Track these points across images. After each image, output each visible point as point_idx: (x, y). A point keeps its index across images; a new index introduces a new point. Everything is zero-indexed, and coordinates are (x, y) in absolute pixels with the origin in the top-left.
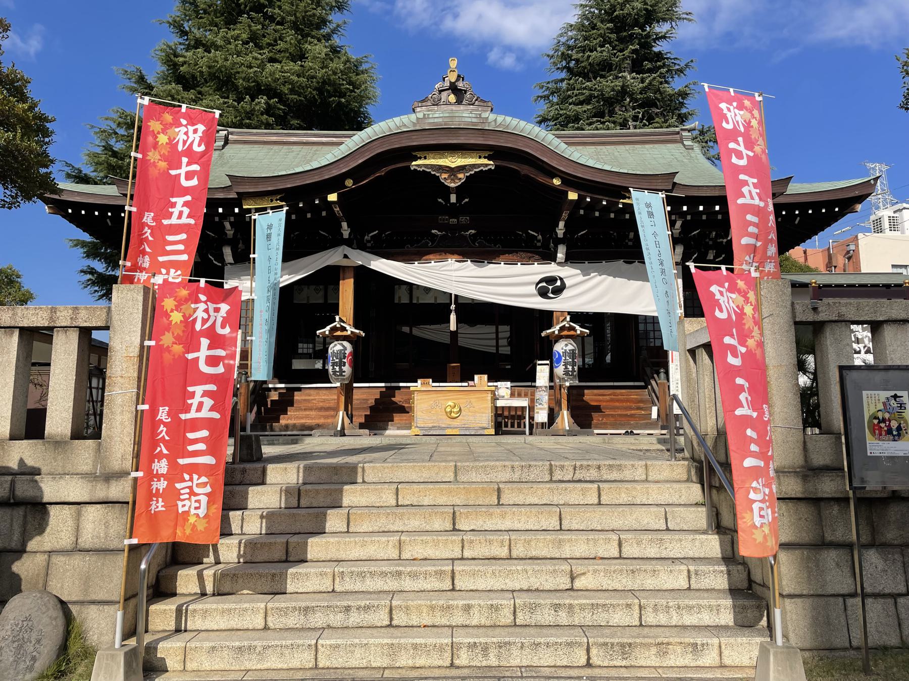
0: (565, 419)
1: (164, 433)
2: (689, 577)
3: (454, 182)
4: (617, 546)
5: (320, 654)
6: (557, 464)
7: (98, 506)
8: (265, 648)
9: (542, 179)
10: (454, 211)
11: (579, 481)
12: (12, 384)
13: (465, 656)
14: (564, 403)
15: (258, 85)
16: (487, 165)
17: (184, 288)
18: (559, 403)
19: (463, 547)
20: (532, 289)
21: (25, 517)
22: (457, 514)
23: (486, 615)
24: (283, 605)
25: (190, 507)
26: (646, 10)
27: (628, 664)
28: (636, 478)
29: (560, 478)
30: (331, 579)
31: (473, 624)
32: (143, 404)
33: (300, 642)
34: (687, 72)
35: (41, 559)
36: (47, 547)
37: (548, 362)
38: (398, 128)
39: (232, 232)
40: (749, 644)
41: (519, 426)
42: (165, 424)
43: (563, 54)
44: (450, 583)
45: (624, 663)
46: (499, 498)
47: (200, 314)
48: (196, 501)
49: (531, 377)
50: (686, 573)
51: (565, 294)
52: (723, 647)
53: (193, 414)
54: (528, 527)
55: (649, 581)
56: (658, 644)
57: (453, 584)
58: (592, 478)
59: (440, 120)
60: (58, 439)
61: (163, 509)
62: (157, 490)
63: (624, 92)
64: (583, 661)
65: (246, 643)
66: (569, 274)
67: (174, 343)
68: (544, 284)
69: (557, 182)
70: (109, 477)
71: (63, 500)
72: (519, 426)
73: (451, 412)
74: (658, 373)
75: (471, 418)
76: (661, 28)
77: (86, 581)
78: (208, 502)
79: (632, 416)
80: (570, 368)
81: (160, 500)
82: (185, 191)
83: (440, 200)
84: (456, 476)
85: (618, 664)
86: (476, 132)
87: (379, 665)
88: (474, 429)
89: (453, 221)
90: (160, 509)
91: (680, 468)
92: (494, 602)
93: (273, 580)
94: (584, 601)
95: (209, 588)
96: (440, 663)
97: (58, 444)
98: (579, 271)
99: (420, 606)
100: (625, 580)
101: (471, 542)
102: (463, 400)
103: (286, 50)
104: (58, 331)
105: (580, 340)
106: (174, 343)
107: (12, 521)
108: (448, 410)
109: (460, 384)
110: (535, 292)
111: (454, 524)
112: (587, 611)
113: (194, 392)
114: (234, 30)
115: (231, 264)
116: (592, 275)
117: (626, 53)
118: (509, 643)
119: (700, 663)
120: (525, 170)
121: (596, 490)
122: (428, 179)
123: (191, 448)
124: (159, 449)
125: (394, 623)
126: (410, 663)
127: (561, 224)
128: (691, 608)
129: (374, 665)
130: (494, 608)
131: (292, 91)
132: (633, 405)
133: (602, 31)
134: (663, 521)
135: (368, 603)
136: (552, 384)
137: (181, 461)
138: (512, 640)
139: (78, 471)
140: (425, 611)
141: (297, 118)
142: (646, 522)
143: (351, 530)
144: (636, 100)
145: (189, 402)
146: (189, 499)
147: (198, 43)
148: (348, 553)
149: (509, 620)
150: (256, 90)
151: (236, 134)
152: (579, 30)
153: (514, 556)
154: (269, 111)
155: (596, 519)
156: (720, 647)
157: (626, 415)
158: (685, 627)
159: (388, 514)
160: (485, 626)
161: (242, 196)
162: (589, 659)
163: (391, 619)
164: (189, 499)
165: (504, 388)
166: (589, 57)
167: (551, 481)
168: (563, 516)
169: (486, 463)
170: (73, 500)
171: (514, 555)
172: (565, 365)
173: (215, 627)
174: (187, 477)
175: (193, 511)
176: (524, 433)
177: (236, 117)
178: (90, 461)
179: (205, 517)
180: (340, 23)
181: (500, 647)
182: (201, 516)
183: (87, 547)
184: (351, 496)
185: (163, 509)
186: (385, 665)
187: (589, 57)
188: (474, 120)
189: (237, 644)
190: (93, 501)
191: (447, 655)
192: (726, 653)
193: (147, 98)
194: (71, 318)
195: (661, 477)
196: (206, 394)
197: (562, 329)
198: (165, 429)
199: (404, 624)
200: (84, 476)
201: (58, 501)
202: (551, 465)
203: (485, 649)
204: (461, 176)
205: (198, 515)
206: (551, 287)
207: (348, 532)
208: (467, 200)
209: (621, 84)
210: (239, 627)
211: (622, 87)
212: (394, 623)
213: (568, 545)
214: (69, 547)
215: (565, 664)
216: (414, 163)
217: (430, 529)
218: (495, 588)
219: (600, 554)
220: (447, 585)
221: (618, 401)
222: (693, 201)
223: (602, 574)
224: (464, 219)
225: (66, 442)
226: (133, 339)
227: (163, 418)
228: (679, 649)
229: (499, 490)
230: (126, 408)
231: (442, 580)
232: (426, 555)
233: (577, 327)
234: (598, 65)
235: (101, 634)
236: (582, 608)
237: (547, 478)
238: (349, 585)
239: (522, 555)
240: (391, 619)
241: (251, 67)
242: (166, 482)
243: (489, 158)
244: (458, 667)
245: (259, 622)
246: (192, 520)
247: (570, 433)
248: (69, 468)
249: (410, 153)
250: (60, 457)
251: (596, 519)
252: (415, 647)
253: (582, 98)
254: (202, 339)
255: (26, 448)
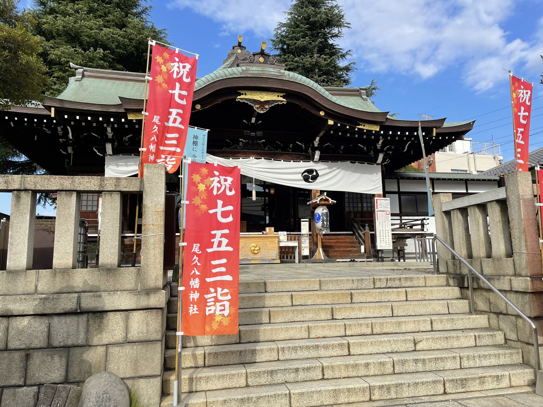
0: (320, 253)
1: (196, 261)
2: (475, 339)
3: (263, 110)
4: (430, 324)
5: (292, 399)
6: (378, 277)
7: (141, 311)
8: (258, 398)
9: (313, 111)
10: (254, 127)
11: (390, 288)
12: (73, 230)
13: (377, 394)
14: (320, 245)
15: (96, 41)
16: (282, 101)
17: (205, 167)
18: (316, 244)
19: (345, 329)
20: (300, 177)
21: (88, 321)
22: (334, 309)
23: (378, 368)
24: (257, 370)
25: (215, 310)
26: (328, 19)
27: (465, 391)
28: (420, 285)
29: (379, 286)
30: (276, 352)
31: (371, 374)
32: (183, 242)
33: (280, 393)
34: (347, 57)
35: (101, 350)
36: (105, 341)
37: (308, 220)
38: (231, 75)
39: (112, 134)
40: (523, 373)
41: (291, 258)
42: (198, 255)
43: (281, 40)
44: (347, 351)
45: (463, 390)
46: (351, 299)
47: (215, 184)
48: (220, 306)
49: (298, 228)
50: (474, 337)
51: (319, 180)
52: (511, 376)
53: (215, 248)
54: (376, 315)
55: (455, 343)
56: (480, 378)
57: (349, 351)
58: (396, 286)
59: (257, 72)
60: (109, 267)
61: (198, 312)
62: (193, 299)
63: (316, 64)
64: (442, 391)
65: (246, 396)
66: (321, 168)
67: (201, 204)
68: (306, 174)
69: (322, 113)
70: (149, 292)
71: (117, 308)
72: (291, 258)
73: (254, 250)
74: (364, 227)
75: (266, 253)
76: (335, 30)
77: (136, 363)
78: (230, 306)
79: (350, 251)
80: (325, 223)
81: (195, 306)
82: (179, 106)
83: (244, 121)
84: (320, 286)
85: (460, 391)
86: (279, 81)
87: (328, 403)
88: (268, 260)
89: (253, 134)
90: (195, 312)
91: (442, 279)
92: (382, 360)
93: (240, 355)
94: (431, 357)
95: (201, 362)
96: (364, 399)
97: (109, 270)
98: (326, 167)
99: (340, 365)
100: (443, 343)
101: (350, 325)
102: (261, 243)
103: (113, 21)
104: (106, 194)
105: (329, 207)
106: (201, 204)
107: (78, 325)
108: (252, 249)
109: (248, 233)
110: (302, 178)
111: (333, 315)
112: (432, 362)
113: (215, 234)
114: (78, 4)
115: (110, 155)
116: (334, 169)
117: (317, 43)
118: (402, 384)
119: (500, 386)
120: (304, 105)
121: (405, 292)
122: (247, 109)
123: (214, 271)
124: (193, 271)
125: (325, 377)
126: (346, 400)
127: (318, 139)
128: (485, 356)
129: (325, 404)
130: (382, 364)
131: (118, 47)
132: (350, 245)
133: (303, 29)
134: (446, 309)
135: (309, 365)
136: (311, 233)
137: (208, 280)
138: (403, 382)
139: (124, 288)
140: (343, 368)
141: (119, 64)
142: (437, 310)
143: (271, 322)
144: (322, 70)
145: (212, 240)
146: (214, 305)
147: (52, 11)
148: (278, 335)
149: (391, 370)
150: (97, 44)
151: (89, 71)
152: (289, 27)
153: (375, 333)
154: (104, 58)
155: (411, 308)
156: (510, 376)
157: (347, 251)
158: (483, 367)
159: (294, 311)
160: (377, 375)
161: (128, 111)
162: (445, 389)
163: (323, 375)
164: (214, 305)
165: (283, 235)
166: (296, 43)
167: (374, 288)
168: (393, 308)
169: (338, 278)
170: (124, 308)
171: (375, 332)
172: (323, 221)
173: (214, 388)
174: (212, 290)
175: (218, 313)
176: (294, 262)
177: (83, 61)
178: (133, 282)
179: (228, 316)
180: (148, 6)
181: (397, 387)
182: (226, 315)
183: (134, 339)
184: (270, 301)
185: (198, 312)
186: (332, 403)
187: (296, 43)
188: (277, 74)
189: (240, 397)
190: (139, 308)
191: (367, 394)
192: (512, 379)
193: (154, 42)
194: (115, 185)
195: (433, 284)
196: (223, 236)
197: (321, 200)
198: (197, 258)
199: (331, 377)
200: (131, 291)
201: (114, 309)
202: (374, 278)
203: (389, 388)
204: (267, 107)
205: (223, 315)
206: (310, 176)
207: (270, 323)
208: (260, 122)
209: (315, 60)
210: (230, 386)
211: (316, 62)
212: (325, 377)
213: (404, 325)
214: (121, 341)
215: (432, 393)
216: (238, 97)
217: (319, 319)
218: (373, 352)
219: (422, 329)
220: (346, 352)
221: (340, 242)
222: (395, 129)
223: (431, 340)
224: (259, 133)
225: (115, 269)
226: (160, 199)
227: (196, 251)
228: (490, 379)
229: (351, 294)
230: (157, 245)
231: (342, 350)
232: (324, 335)
233: (330, 199)
234: (301, 49)
235: (150, 398)
236: (430, 360)
237: (372, 286)
238: (287, 356)
239: (379, 332)
240: (323, 375)
241: (91, 29)
242: (199, 294)
243: (283, 97)
244: (374, 401)
245: (243, 382)
246: (218, 319)
247: (326, 262)
248: (118, 286)
249: (235, 91)
250: (111, 280)
251: (411, 308)
252: (349, 390)
253: (292, 67)
254: (218, 201)
255: (86, 274)
